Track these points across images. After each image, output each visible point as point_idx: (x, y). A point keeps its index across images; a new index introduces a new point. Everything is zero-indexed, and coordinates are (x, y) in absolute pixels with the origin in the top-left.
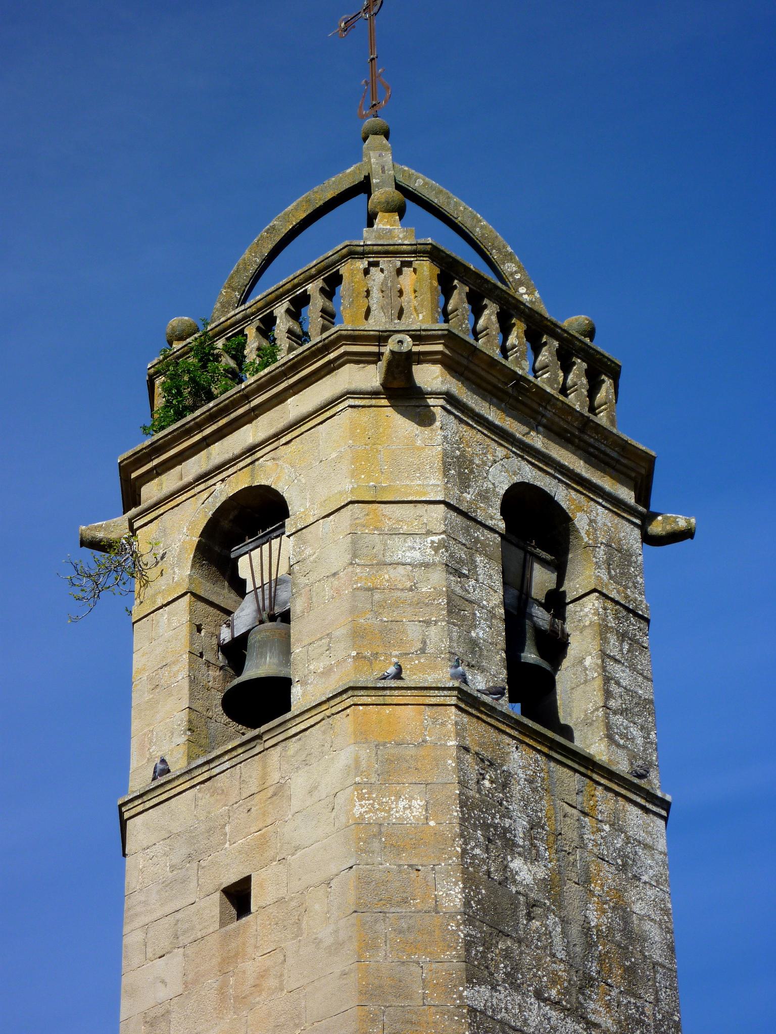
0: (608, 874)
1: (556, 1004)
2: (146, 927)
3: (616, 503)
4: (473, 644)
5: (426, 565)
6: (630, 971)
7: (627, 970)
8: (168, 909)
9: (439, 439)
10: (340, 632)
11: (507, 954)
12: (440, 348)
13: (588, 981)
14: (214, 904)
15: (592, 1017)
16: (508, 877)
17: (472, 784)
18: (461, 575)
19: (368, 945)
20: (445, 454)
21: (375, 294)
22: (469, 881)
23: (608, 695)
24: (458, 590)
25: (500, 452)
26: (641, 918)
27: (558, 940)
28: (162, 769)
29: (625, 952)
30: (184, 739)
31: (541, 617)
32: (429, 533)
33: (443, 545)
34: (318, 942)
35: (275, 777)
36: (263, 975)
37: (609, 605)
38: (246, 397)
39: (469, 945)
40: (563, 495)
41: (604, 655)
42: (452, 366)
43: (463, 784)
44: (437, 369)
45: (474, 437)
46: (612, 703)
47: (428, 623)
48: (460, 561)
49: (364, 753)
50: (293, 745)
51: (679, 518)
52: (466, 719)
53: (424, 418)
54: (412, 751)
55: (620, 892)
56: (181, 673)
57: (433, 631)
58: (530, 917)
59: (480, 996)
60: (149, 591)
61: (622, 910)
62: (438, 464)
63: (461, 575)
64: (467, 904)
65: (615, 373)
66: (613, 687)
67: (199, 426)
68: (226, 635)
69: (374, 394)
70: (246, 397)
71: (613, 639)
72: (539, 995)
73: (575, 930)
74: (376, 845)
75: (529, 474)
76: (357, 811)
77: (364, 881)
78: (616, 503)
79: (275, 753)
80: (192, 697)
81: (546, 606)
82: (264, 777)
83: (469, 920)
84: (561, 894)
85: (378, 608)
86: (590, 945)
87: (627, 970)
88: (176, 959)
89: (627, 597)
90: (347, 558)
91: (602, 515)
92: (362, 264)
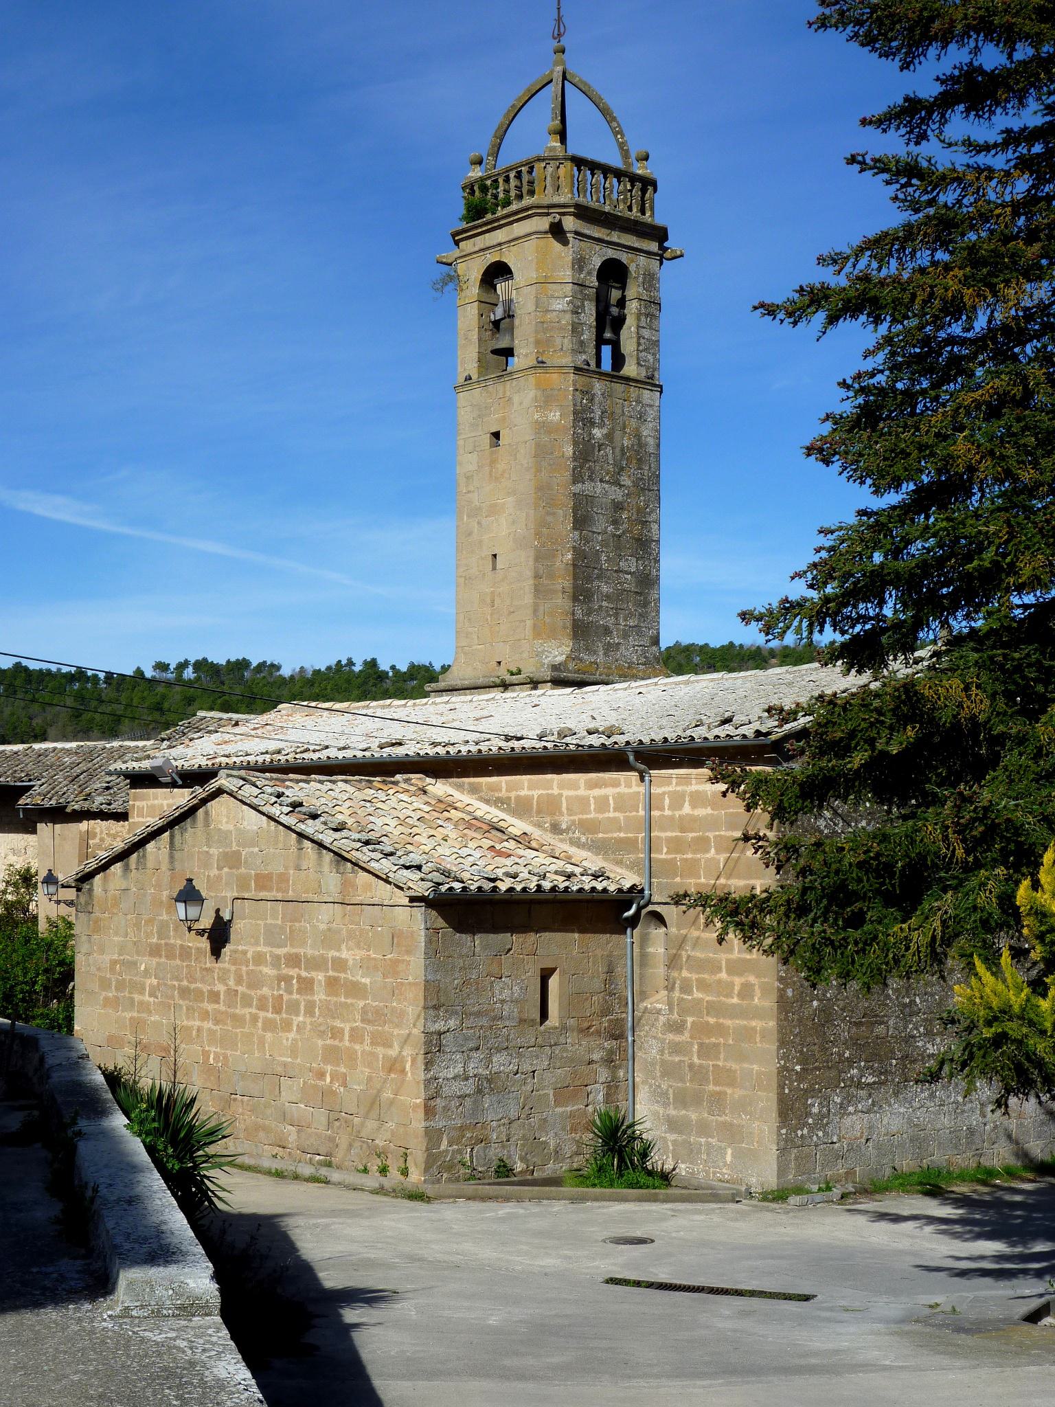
0: (633, 423)
1: (607, 482)
2: (465, 439)
3: (649, 253)
4: (582, 343)
5: (564, 311)
6: (640, 461)
7: (638, 460)
8: (473, 434)
9: (571, 253)
10: (532, 340)
11: (589, 468)
12: (572, 210)
13: (622, 469)
14: (487, 439)
15: (622, 483)
16: (591, 436)
17: (579, 404)
18: (578, 313)
19: (539, 470)
20: (573, 258)
21: (549, 178)
22: (575, 444)
23: (639, 344)
24: (577, 321)
25: (598, 248)
26: (646, 437)
27: (610, 456)
28: (469, 378)
29: (638, 452)
30: (476, 365)
31: (615, 311)
32: (566, 297)
33: (571, 302)
34: (522, 465)
35: (508, 394)
36: (504, 471)
37: (642, 303)
38: (498, 220)
39: (574, 470)
40: (624, 257)
41: (638, 327)
42: (577, 216)
43: (575, 405)
44: (571, 218)
45: (586, 245)
46: (641, 348)
47: (564, 337)
48: (578, 307)
49: (539, 393)
50: (514, 382)
51: (334, 1223)
52: (577, 377)
53: (565, 242)
54: (556, 392)
55: (637, 429)
56: (474, 336)
57: (566, 341)
58: (599, 451)
59: (578, 488)
60: (463, 294)
61: (638, 436)
62: (570, 265)
63: (578, 313)
64: (574, 453)
65: (654, 184)
66: (642, 341)
67: (481, 226)
68: (492, 318)
69: (546, 233)
70: (498, 220)
71: (643, 318)
72: (601, 481)
73: (618, 450)
74: (542, 431)
75: (611, 253)
76: (536, 417)
77: (538, 445)
78: (649, 253)
79: (508, 383)
80: (480, 346)
81: (617, 306)
82: (504, 392)
83: (575, 460)
84: (613, 438)
85: (545, 331)
86: (623, 454)
87: (638, 460)
88: (475, 455)
89: (651, 296)
90: (534, 308)
91: (642, 260)
92: (543, 164)
